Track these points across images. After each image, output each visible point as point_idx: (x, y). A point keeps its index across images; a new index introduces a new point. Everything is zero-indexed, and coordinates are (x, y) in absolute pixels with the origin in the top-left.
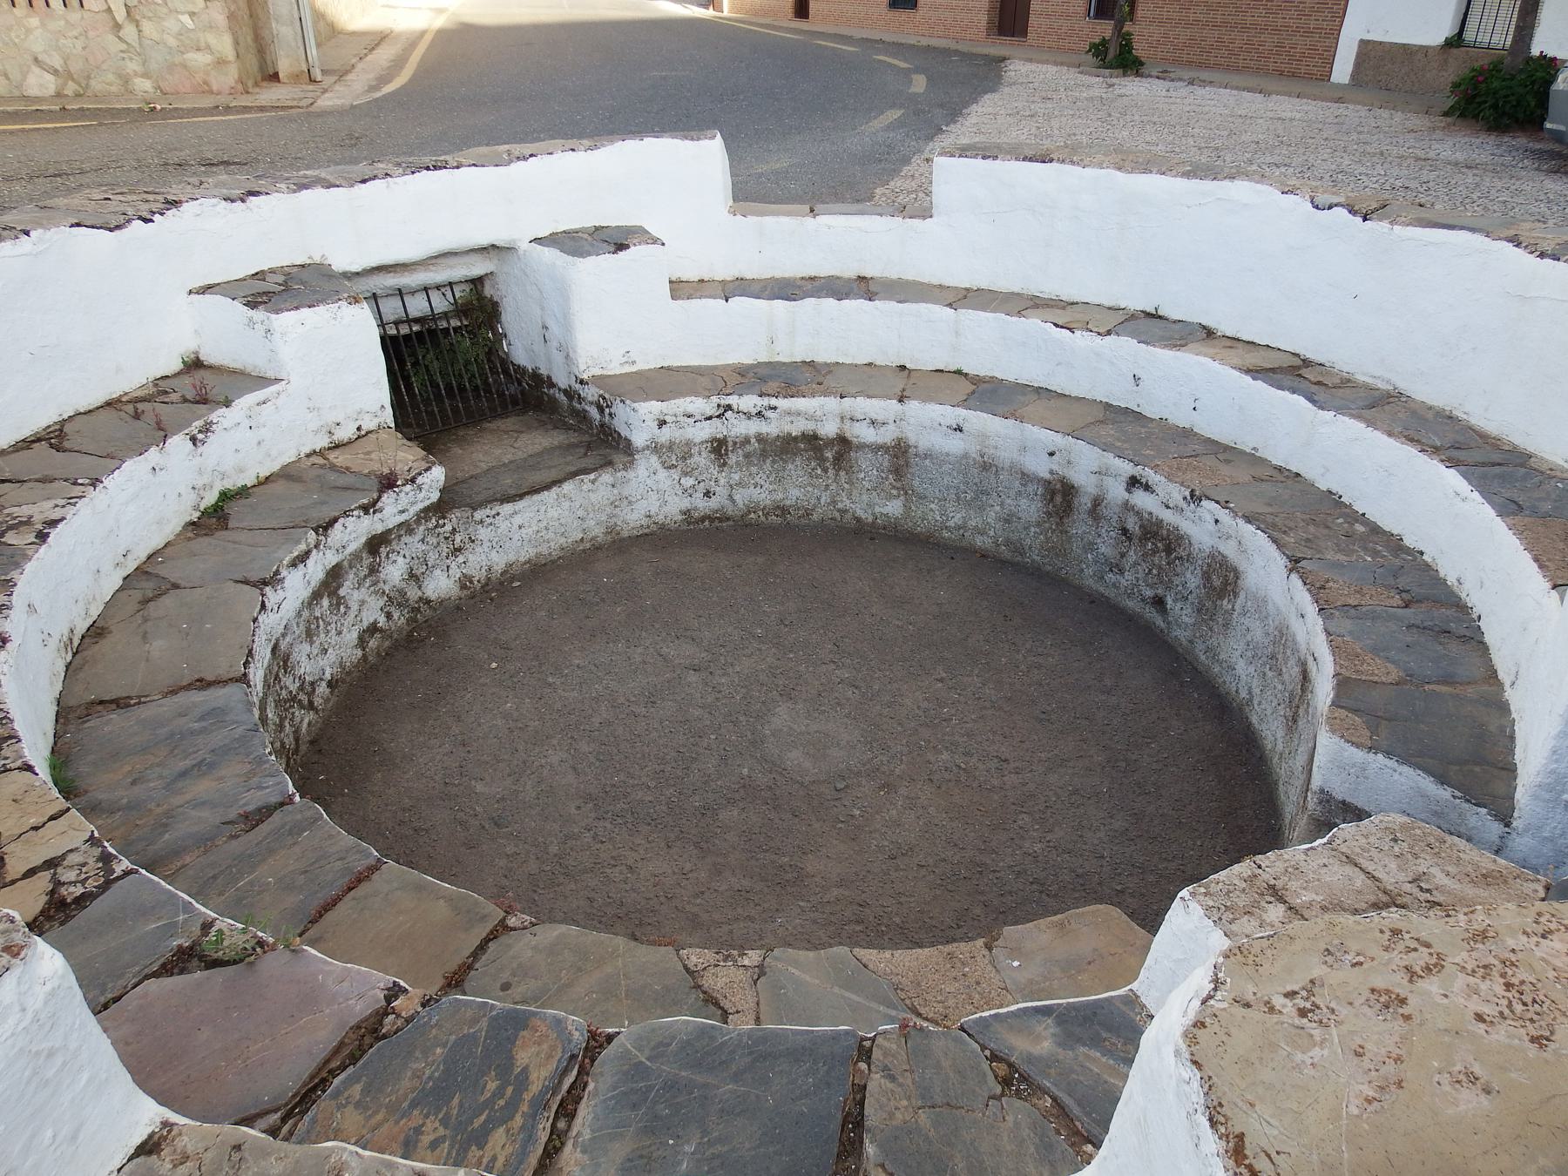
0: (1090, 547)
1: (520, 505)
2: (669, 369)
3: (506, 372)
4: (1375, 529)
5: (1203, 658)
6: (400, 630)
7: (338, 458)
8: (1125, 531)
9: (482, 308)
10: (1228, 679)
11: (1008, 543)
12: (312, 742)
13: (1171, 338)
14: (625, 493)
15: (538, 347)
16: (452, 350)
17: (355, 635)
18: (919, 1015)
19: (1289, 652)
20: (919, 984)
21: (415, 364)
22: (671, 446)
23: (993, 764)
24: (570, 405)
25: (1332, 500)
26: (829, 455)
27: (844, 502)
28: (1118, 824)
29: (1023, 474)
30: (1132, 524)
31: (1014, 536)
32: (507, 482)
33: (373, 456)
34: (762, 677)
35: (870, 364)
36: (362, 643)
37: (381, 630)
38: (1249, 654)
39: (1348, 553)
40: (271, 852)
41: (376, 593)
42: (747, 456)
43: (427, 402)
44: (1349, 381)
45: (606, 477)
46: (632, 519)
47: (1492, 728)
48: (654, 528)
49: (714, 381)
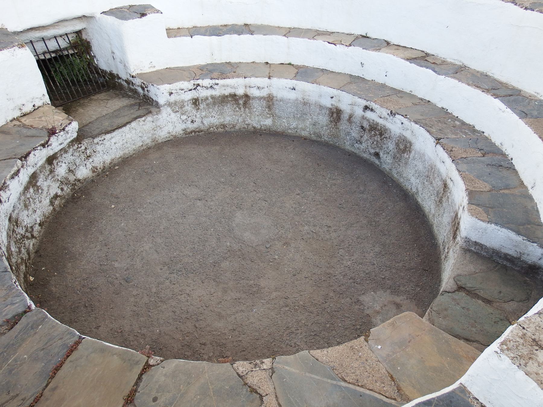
0: (348, 134)
1: (114, 134)
2: (170, 68)
3: (98, 73)
4: (463, 123)
5: (396, 176)
6: (68, 194)
7: (26, 121)
8: (362, 127)
9: (82, 45)
10: (407, 184)
11: (315, 133)
12: (36, 252)
13: (374, 46)
14: (158, 124)
15: (111, 61)
16: (71, 64)
17: (48, 201)
18: (345, 381)
19: (436, 176)
20: (342, 365)
21: (55, 71)
22: (175, 103)
23: (325, 229)
24: (129, 87)
25: (443, 110)
26: (241, 102)
27: (249, 121)
28: (377, 249)
29: (320, 106)
30: (366, 125)
31: (317, 131)
32: (106, 124)
33: (43, 119)
34: (228, 201)
35: (253, 62)
36: (52, 203)
37: (60, 196)
38: (417, 175)
39: (456, 134)
40: (23, 340)
41: (54, 181)
42: (207, 105)
43: (64, 89)
44: (444, 61)
45: (149, 118)
46: (163, 135)
47: (529, 207)
48: (172, 137)
49: (190, 73)
